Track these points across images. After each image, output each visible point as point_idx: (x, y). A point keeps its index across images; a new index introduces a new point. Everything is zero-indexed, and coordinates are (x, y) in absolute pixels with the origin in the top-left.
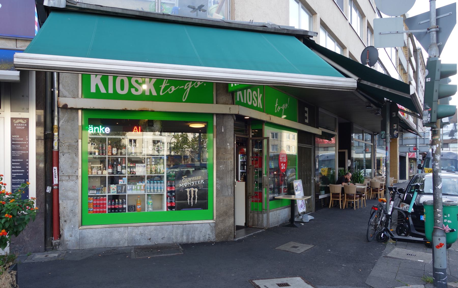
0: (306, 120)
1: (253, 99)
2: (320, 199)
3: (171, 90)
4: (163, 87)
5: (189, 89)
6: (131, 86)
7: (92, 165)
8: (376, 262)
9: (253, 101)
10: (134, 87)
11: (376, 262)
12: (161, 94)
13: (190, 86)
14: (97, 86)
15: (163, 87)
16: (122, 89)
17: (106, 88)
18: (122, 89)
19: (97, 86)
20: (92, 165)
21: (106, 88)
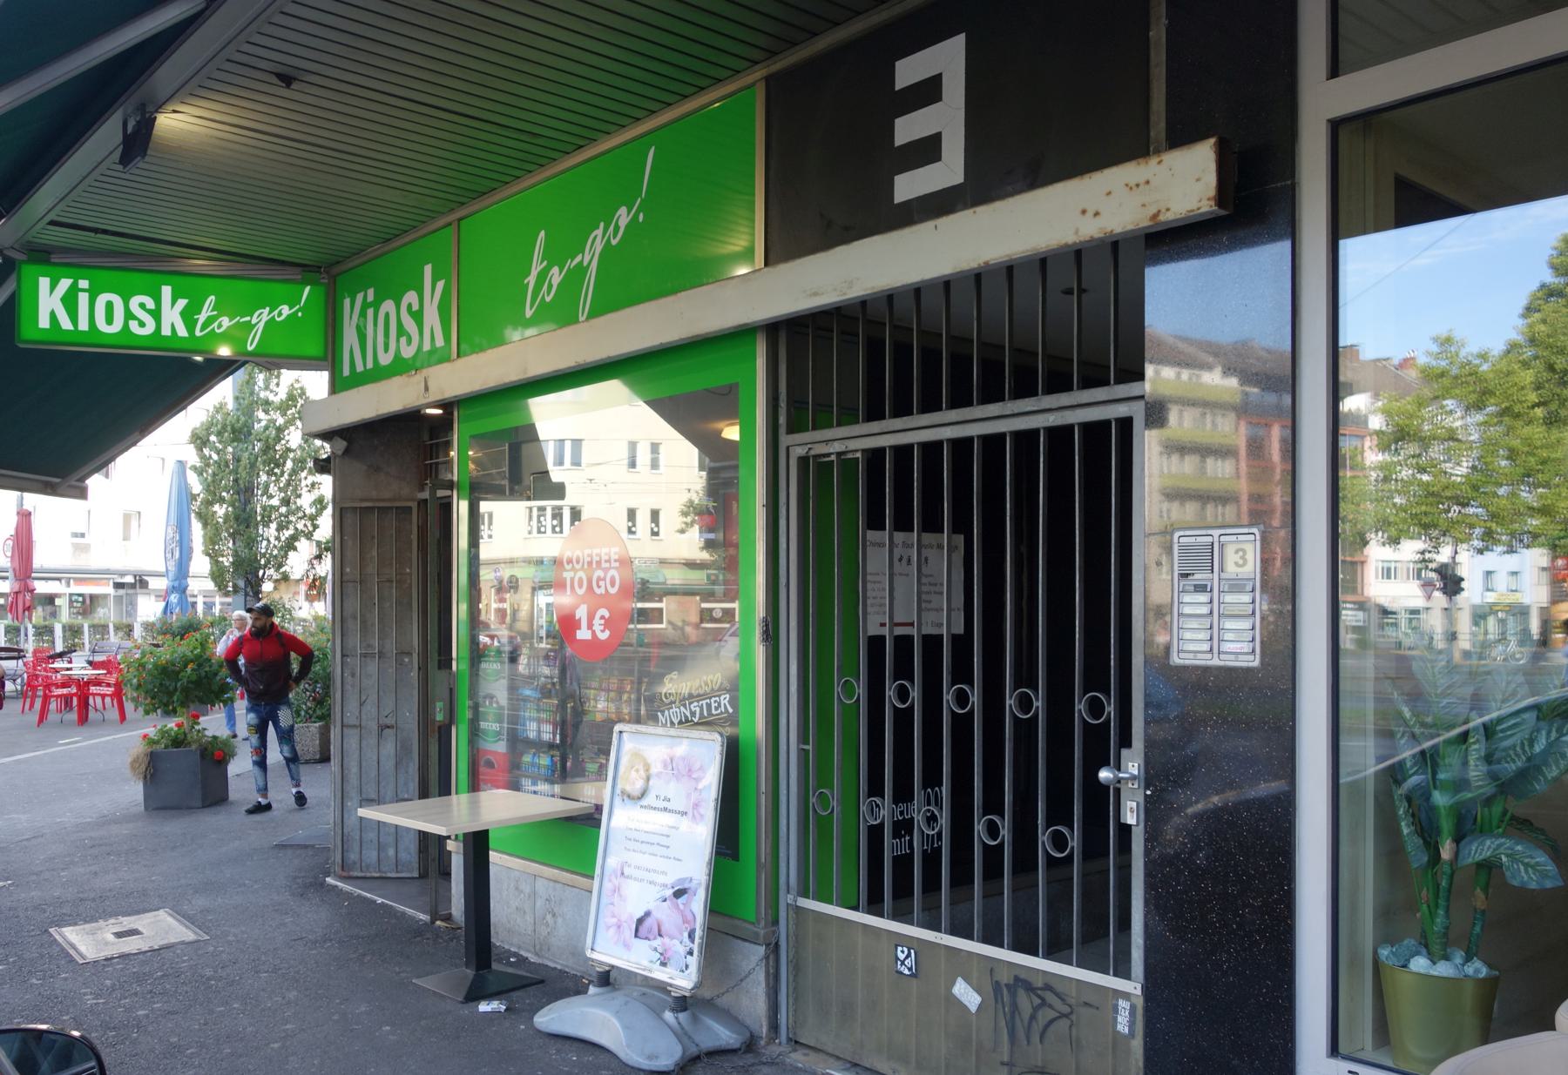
0: (623, 210)
1: (401, 331)
2: (1179, 138)
3: (220, 326)
4: (202, 318)
5: (261, 325)
6: (129, 315)
7: (704, 605)
8: (1147, 788)
9: (403, 340)
10: (135, 318)
11: (1147, 788)
12: (198, 333)
13: (265, 318)
14: (53, 314)
15: (202, 318)
16: (109, 321)
17: (74, 317)
18: (109, 321)
19: (53, 314)
20: (704, 605)
21: (74, 317)
